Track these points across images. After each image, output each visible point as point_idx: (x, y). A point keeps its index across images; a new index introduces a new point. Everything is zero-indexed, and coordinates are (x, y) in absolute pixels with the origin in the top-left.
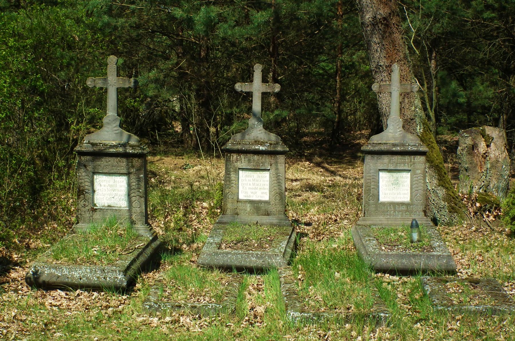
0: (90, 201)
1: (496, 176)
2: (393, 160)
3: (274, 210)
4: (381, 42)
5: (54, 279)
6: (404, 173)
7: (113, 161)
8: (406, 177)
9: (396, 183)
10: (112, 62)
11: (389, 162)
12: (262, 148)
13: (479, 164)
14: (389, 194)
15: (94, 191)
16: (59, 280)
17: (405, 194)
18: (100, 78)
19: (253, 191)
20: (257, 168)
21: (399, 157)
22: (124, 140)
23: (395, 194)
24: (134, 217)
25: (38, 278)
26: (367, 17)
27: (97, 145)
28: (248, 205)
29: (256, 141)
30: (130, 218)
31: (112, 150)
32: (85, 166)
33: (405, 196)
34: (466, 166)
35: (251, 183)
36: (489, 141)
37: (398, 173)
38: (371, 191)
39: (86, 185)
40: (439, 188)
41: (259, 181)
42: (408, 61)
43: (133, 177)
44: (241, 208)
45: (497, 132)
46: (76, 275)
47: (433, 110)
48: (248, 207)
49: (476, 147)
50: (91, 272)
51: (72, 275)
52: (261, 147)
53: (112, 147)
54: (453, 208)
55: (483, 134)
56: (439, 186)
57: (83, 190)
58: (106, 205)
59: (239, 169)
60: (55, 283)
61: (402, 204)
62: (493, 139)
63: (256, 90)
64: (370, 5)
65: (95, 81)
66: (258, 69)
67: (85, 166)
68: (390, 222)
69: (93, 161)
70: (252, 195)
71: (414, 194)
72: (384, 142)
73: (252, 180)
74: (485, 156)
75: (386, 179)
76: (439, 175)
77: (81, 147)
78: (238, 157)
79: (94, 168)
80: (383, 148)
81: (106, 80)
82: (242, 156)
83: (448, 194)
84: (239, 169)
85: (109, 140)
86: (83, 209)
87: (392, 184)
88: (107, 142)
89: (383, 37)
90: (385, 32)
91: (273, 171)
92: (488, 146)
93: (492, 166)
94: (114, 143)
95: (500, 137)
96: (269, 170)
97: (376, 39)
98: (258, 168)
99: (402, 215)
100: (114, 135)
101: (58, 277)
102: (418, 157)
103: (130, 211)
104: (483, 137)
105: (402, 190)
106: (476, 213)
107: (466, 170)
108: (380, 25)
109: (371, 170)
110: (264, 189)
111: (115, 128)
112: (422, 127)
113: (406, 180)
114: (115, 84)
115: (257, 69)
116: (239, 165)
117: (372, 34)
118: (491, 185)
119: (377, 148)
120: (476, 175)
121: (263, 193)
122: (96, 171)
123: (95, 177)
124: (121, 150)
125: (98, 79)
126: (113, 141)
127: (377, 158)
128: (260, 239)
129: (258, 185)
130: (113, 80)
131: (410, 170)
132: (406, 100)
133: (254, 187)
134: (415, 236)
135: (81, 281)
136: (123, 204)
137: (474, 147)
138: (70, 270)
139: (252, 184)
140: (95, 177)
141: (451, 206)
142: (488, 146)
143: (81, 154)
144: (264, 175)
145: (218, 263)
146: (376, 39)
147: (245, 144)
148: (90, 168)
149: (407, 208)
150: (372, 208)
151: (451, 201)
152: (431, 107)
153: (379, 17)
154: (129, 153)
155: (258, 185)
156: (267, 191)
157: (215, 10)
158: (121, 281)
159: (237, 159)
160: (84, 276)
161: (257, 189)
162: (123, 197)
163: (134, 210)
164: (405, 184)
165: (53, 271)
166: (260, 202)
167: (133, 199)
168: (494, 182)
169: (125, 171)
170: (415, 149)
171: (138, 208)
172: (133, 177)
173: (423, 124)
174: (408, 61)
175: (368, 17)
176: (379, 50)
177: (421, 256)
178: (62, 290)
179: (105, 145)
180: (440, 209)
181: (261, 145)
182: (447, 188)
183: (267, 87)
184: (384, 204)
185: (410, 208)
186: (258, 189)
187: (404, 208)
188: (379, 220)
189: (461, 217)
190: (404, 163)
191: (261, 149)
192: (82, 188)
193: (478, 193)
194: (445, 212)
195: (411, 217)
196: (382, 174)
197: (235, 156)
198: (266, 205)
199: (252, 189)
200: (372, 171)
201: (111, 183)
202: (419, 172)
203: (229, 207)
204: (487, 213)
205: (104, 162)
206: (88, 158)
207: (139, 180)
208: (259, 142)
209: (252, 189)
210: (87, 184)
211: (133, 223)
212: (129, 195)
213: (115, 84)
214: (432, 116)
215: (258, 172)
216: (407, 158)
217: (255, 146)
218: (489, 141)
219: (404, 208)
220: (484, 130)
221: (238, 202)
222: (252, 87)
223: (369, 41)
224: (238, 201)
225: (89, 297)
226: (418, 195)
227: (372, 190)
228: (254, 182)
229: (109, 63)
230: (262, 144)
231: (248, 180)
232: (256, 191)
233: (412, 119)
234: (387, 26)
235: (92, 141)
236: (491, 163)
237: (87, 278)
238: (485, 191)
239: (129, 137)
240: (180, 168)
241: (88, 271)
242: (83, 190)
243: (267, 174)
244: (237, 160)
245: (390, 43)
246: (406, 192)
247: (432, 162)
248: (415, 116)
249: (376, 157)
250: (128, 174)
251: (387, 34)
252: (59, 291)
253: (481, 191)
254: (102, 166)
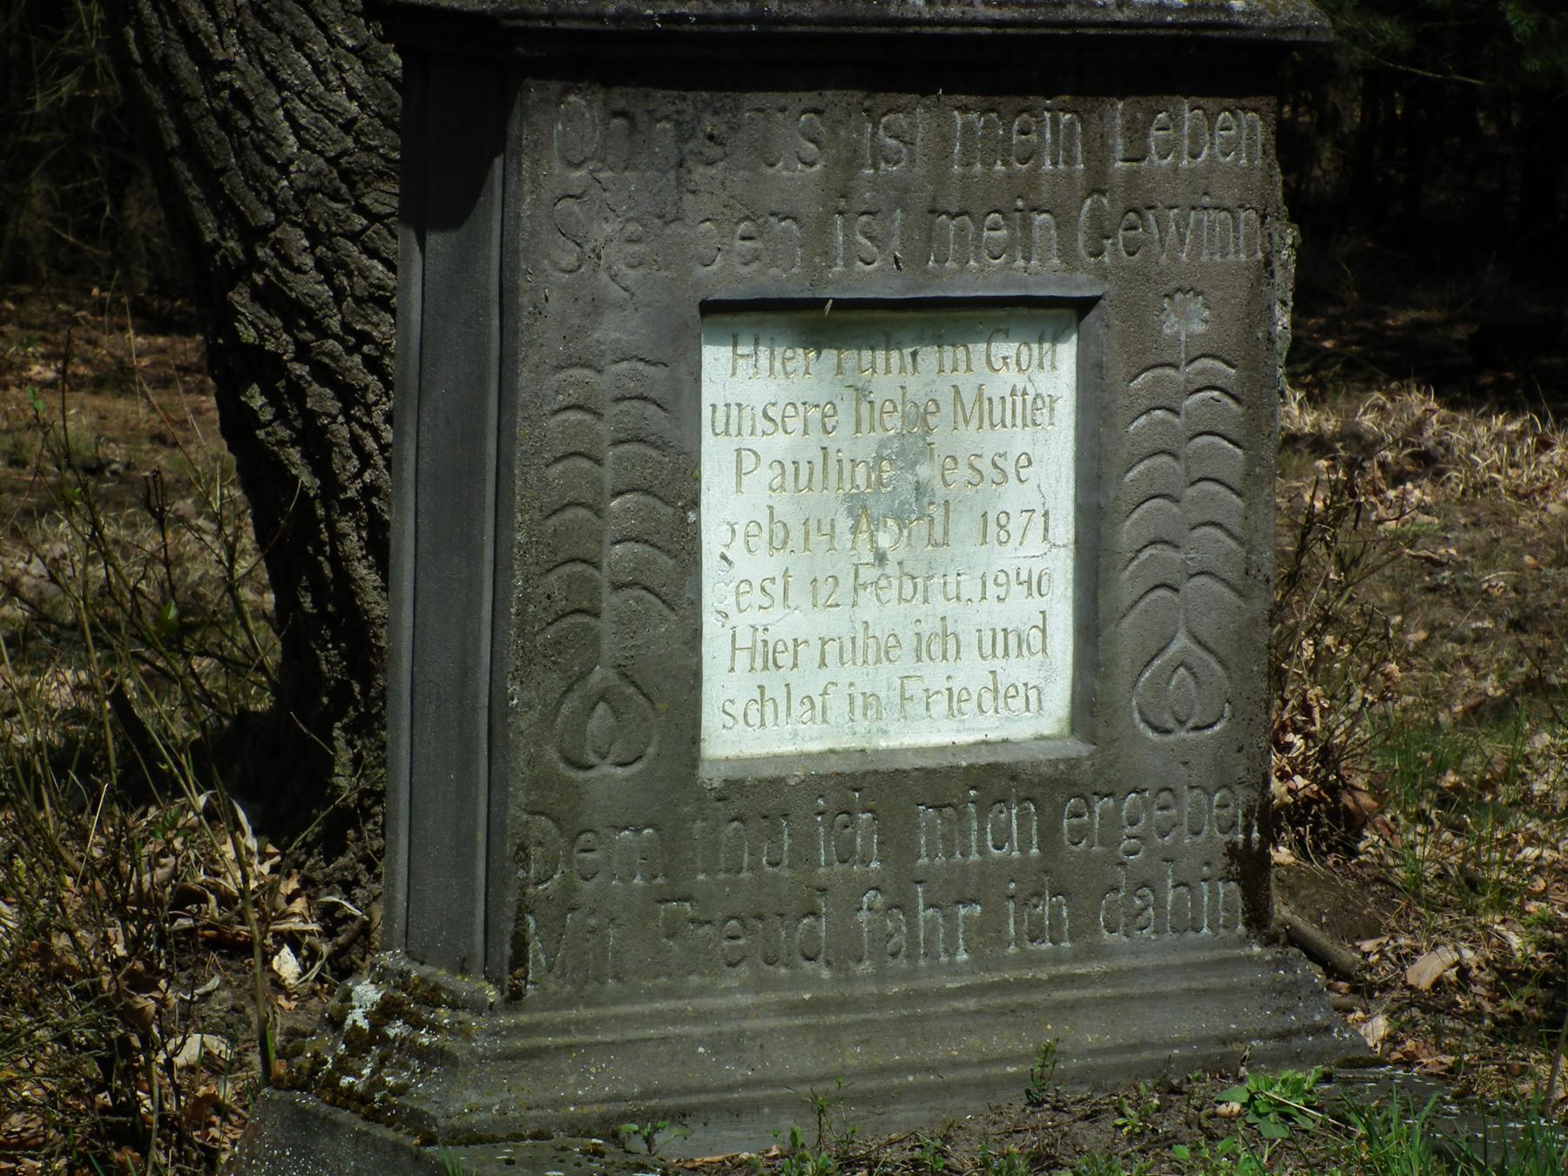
2: (880, 154)
6: (1004, 349)
14: (809, 655)
17: (1007, 642)
23: (884, 654)
31: (860, 1085)
33: (1017, 670)
37: (929, 356)
38: (605, 625)
68: (854, 1056)
71: (1128, 633)
75: (778, 445)
87: (858, 508)
99: (987, 934)
102: (1189, 114)
105: (970, 588)
109: (596, 307)
113: (1019, 440)
127: (684, 133)
128: (1467, 660)
131: (1083, 307)
145: (1059, 720)
149: (1049, 835)
164: (1013, 497)
185: (1080, 833)
188: (714, 1042)
195: (1095, 952)
200: (611, 332)
226: (1181, 642)
227: (611, 601)
246: (1020, 610)
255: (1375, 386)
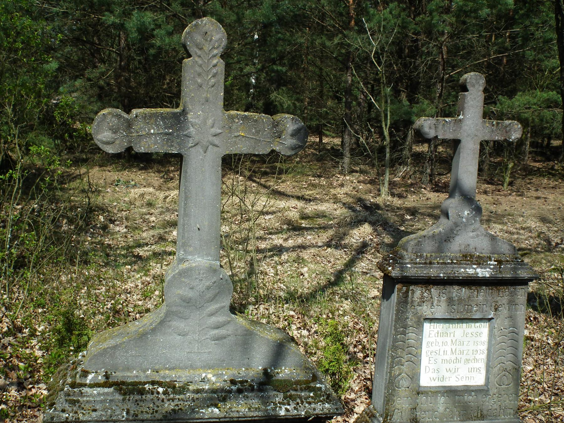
3: (495, 406)
10: (207, 47)
12: (483, 273)
18: (152, 116)
19: (452, 366)
20: (466, 317)
27: (142, 392)
28: (442, 400)
29: (465, 256)
35: (448, 349)
41: (465, 343)
44: (424, 406)
47: (387, 129)
48: (441, 403)
52: (479, 270)
59: (426, 319)
63: (469, 135)
65: (129, 125)
66: (477, 86)
70: (447, 375)
73: (449, 342)
77: (73, 403)
78: (425, 294)
82: (434, 291)
84: (426, 319)
85: (192, 367)
91: (501, 322)
96: (490, 320)
98: (468, 316)
110: (476, 360)
111: (214, 320)
114: (216, 141)
115: (473, 86)
116: (426, 310)
121: (471, 370)
125: (145, 117)
126: (207, 367)
129: (462, 353)
130: (210, 122)
133: (453, 357)
139: (449, 352)
144: (478, 330)
147: (442, 263)
152: (386, 125)
155: (462, 353)
156: (482, 366)
157: (149, 17)
159: (423, 297)
161: (460, 362)
166: (467, 390)
181: (479, 264)
183: (494, 128)
186: (463, 362)
191: (480, 275)
197: (417, 292)
198: (480, 397)
199: (449, 361)
203: (399, 407)
208: (472, 256)
209: (449, 361)
213: (216, 141)
214: (386, 136)
215: (464, 325)
217: (465, 268)
221: (418, 393)
222: (461, 128)
224: (419, 392)
228: (454, 348)
229: (192, 50)
230: (481, 261)
231: (441, 344)
232: (458, 365)
235: (118, 376)
240: (112, 184)
243: (484, 329)
244: (422, 301)
255: (421, 389)
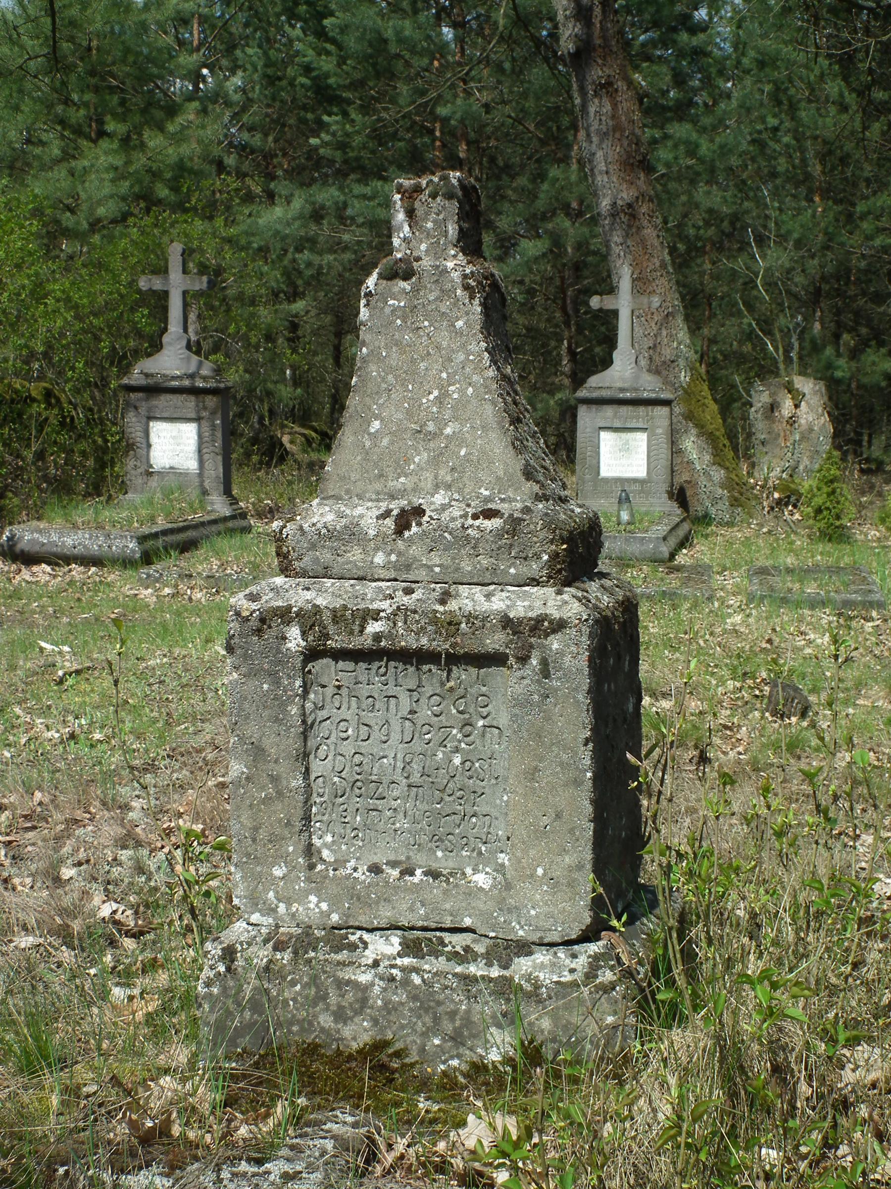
0: (144, 460)
1: (808, 454)
4: (625, 242)
5: (37, 548)
7: (177, 399)
8: (641, 439)
9: (626, 449)
11: (615, 416)
13: (782, 434)
15: (149, 446)
16: (44, 549)
21: (630, 408)
22: (192, 369)
24: (207, 484)
25: (14, 545)
26: (604, 203)
30: (201, 485)
31: (175, 383)
32: (136, 408)
34: (763, 437)
36: (798, 399)
39: (136, 434)
40: (714, 468)
42: (668, 273)
43: (205, 423)
45: (811, 385)
46: (69, 542)
49: (778, 407)
50: (90, 539)
51: (63, 542)
53: (174, 378)
54: (736, 500)
55: (790, 388)
56: (714, 464)
57: (133, 444)
58: (167, 466)
60: (38, 553)
61: (635, 481)
62: (804, 395)
64: (608, 186)
67: (136, 408)
69: (147, 399)
72: (607, 384)
74: (792, 421)
76: (714, 448)
79: (149, 410)
80: (605, 394)
81: (166, 279)
83: (728, 478)
86: (133, 472)
88: (168, 372)
89: (627, 235)
90: (630, 226)
92: (797, 406)
93: (803, 438)
94: (178, 373)
95: (815, 393)
97: (616, 238)
100: (178, 362)
101: (43, 544)
102: (659, 408)
103: (201, 475)
104: (790, 392)
106: (772, 508)
107: (763, 443)
108: (622, 216)
112: (689, 374)
117: (611, 230)
118: (801, 467)
119: (595, 395)
120: (777, 451)
122: (152, 415)
123: (151, 424)
124: (187, 383)
132: (664, 333)
134: (625, 516)
135: (76, 551)
136: (192, 465)
137: (773, 407)
138: (61, 535)
140: (151, 424)
141: (733, 496)
142: (797, 406)
143: (130, 389)
146: (616, 238)
148: (143, 411)
150: (589, 486)
151: (733, 489)
153: (620, 203)
154: (199, 388)
158: (133, 551)
160: (79, 544)
162: (191, 455)
163: (206, 473)
165: (36, 535)
167: (206, 457)
168: (805, 462)
169: (193, 415)
170: (654, 395)
171: (214, 469)
172: (205, 423)
173: (691, 369)
174: (668, 273)
175: (605, 204)
176: (622, 254)
177: (615, 537)
178: (49, 564)
179: (164, 375)
180: (715, 501)
182: (727, 468)
184: (606, 480)
187: (637, 487)
189: (748, 513)
190: (637, 418)
192: (131, 441)
193: (780, 478)
194: (725, 505)
196: (604, 435)
201: (174, 434)
202: (659, 431)
204: (790, 508)
205: (163, 402)
206: (140, 395)
207: (213, 427)
210: (139, 434)
211: (205, 493)
212: (200, 451)
216: (642, 410)
218: (798, 399)
219: (637, 487)
220: (790, 383)
223: (608, 241)
225: (84, 573)
233: (673, 362)
234: (633, 216)
235: (145, 371)
236: (801, 433)
237: (85, 546)
238: (791, 476)
239: (200, 364)
241: (87, 536)
242: (133, 444)
245: (638, 244)
247: (702, 427)
248: (678, 356)
249: (594, 407)
250: (198, 420)
251: (634, 230)
252: (43, 565)
253: (784, 475)
254: (161, 407)
